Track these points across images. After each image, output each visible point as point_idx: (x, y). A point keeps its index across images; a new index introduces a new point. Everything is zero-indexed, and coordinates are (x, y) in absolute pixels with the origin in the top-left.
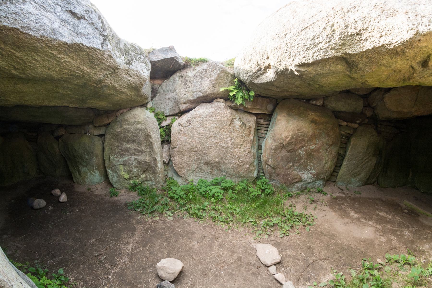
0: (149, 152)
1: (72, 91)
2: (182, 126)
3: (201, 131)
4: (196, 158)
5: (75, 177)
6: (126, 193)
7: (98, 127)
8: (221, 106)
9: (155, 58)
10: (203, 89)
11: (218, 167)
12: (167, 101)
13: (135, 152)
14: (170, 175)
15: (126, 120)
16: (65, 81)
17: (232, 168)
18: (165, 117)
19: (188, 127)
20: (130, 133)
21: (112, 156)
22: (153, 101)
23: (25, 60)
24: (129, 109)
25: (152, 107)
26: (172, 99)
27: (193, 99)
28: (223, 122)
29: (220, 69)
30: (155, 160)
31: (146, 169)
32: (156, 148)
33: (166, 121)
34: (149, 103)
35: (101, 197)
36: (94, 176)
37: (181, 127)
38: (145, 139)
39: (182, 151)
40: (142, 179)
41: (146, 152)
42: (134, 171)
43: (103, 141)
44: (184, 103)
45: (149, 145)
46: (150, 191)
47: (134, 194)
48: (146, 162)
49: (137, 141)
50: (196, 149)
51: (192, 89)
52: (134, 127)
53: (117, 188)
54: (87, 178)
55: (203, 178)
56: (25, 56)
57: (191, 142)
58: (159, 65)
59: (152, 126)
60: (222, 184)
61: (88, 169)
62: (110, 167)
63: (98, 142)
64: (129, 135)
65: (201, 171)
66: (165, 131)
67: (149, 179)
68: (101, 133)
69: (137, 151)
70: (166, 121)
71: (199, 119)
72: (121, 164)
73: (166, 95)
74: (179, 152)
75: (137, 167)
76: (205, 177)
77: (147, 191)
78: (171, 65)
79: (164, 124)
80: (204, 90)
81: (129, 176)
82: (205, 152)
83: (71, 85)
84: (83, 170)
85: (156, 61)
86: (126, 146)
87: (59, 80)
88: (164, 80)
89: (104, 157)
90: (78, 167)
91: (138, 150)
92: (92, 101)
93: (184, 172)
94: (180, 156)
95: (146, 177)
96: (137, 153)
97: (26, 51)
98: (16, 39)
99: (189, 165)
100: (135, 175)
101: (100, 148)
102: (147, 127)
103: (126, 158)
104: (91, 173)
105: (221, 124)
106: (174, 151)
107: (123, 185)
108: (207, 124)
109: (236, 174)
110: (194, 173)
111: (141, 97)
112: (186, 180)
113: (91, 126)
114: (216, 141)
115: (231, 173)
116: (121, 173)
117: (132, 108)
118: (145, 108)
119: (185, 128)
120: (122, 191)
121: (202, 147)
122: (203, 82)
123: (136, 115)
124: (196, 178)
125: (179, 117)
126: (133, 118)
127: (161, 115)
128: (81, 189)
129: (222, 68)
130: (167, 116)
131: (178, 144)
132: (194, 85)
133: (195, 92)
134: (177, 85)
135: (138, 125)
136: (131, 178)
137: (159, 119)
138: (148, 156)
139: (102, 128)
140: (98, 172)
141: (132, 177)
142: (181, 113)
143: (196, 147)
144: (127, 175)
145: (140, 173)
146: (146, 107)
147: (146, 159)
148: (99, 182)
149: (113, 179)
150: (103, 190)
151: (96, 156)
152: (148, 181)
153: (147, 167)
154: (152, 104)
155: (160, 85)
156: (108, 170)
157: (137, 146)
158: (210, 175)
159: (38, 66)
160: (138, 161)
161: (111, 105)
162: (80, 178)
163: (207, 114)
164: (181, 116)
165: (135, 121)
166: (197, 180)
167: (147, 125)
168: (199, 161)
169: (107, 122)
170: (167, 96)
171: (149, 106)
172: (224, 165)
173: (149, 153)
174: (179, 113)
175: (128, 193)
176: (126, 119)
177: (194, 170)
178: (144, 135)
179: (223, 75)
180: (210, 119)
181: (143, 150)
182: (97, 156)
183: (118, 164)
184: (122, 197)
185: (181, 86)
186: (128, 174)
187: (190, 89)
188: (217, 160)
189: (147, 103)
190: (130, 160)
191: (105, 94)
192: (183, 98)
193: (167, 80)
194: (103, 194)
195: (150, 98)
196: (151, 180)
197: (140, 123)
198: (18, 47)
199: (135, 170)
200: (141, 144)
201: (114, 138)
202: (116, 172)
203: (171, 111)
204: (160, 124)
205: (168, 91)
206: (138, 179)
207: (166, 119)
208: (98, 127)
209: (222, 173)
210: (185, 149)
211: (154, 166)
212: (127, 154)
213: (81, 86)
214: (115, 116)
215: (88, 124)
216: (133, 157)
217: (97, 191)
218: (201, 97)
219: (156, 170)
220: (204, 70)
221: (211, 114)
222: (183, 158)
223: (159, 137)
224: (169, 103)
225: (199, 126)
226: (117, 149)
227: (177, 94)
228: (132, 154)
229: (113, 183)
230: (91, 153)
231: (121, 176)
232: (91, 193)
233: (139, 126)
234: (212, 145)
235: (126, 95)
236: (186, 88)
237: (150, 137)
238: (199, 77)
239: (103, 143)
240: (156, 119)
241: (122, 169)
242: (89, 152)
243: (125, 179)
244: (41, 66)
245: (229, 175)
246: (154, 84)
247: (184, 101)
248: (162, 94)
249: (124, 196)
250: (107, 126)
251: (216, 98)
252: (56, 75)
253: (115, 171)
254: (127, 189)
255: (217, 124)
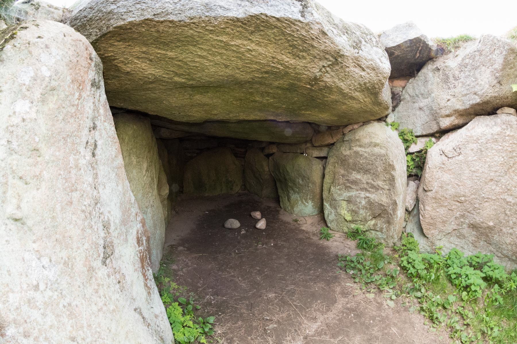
0: (388, 190)
1: (274, 98)
2: (446, 156)
3: (477, 168)
4: (458, 213)
5: (283, 201)
6: (342, 240)
7: (319, 146)
8: (511, 121)
9: (391, 42)
10: (481, 88)
11: (488, 236)
12: (418, 112)
13: (367, 187)
14: (409, 230)
15: (358, 140)
16: (260, 83)
17: (510, 244)
18: (414, 138)
19: (457, 158)
20: (363, 159)
21: (334, 186)
22: (395, 112)
23: (184, 60)
24: (361, 124)
25: (394, 122)
26: (425, 108)
27: (464, 108)
28: (514, 154)
29: (506, 47)
30: (395, 203)
31: (379, 215)
32: (399, 186)
33: (416, 144)
34: (389, 116)
35: (307, 235)
36: (306, 206)
37: (443, 157)
38: (385, 170)
39: (440, 199)
40: (369, 226)
41: (383, 189)
42: (361, 213)
43: (324, 166)
44: (448, 116)
45: (390, 180)
46: (375, 246)
47: (352, 243)
48: (381, 205)
49: (372, 171)
50: (463, 199)
51: (459, 89)
52: (369, 151)
53: (332, 228)
54: (297, 206)
55: (458, 249)
56: (182, 54)
57: (457, 185)
58: (399, 54)
59: (396, 151)
60: (486, 269)
61: (300, 197)
62: (328, 201)
63: (317, 167)
64: (361, 162)
65: (460, 235)
66: (413, 160)
67: (378, 229)
68: (323, 154)
69: (370, 185)
70: (416, 144)
71: (475, 145)
72: (345, 200)
73: (414, 102)
74: (435, 198)
75: (366, 208)
76: (462, 247)
77: (371, 245)
78: (416, 53)
79: (414, 148)
80: (483, 91)
81: (352, 218)
82: (475, 206)
83: (271, 89)
84: (294, 197)
85: (393, 47)
86: (355, 176)
87: (249, 82)
88: (408, 80)
89: (322, 186)
90: (289, 192)
91: (372, 185)
92: (308, 113)
93: (433, 231)
94: (435, 205)
95: (375, 225)
96: (370, 189)
97: (180, 46)
98: (155, 34)
99: (444, 222)
100: (360, 219)
101: (320, 174)
102: (388, 152)
103: (353, 193)
104: (302, 202)
105: (511, 158)
106: (427, 195)
107: (341, 226)
108: (487, 156)
109: (512, 256)
110: (448, 236)
111: (380, 106)
112: (433, 244)
113: (309, 145)
114: (498, 189)
115: (505, 252)
116: (342, 211)
117: (366, 122)
118: (384, 123)
119: (450, 160)
120: (337, 235)
121: (473, 196)
122: (478, 76)
123: (372, 133)
124: (447, 245)
125: (438, 138)
126: (368, 137)
127: (408, 134)
128: (285, 217)
129: (508, 45)
130: (417, 137)
131: (435, 186)
132: (462, 82)
133: (466, 95)
134: (432, 84)
135: (375, 148)
136: (353, 221)
137: (405, 141)
138: (385, 196)
139: (323, 148)
140: (312, 203)
141: (356, 221)
142: (442, 132)
143: (464, 196)
144: (349, 216)
145: (368, 218)
146: (385, 121)
147: (382, 201)
148: (311, 215)
149: (330, 216)
150: (312, 226)
151: (313, 183)
152: (377, 231)
153: (380, 212)
154: (393, 116)
155: (404, 88)
156: (325, 203)
157: (371, 178)
158: (471, 245)
159: (207, 64)
160: (369, 201)
161: (336, 118)
162: (288, 204)
163: (489, 136)
164: (440, 137)
165: (371, 143)
166: (448, 249)
167: (388, 149)
168: (462, 220)
169: (331, 141)
170: (416, 105)
171: (389, 120)
172: (499, 235)
173: (388, 192)
174: (437, 132)
175: (344, 240)
176: (357, 138)
177: (450, 232)
178: (384, 163)
179: (512, 58)
180: (494, 147)
181: (379, 186)
182: (314, 183)
183: (341, 199)
184: (335, 243)
185: (440, 87)
186: (351, 215)
187: (456, 90)
188: (491, 224)
189: (386, 116)
190: (358, 197)
191: (327, 101)
192: (445, 107)
193: (413, 78)
194: (311, 231)
195: (391, 108)
196: (381, 231)
197: (378, 145)
198: (166, 44)
199: (361, 212)
200: (378, 176)
201: (340, 163)
202: (335, 208)
203: (424, 129)
204: (406, 149)
205: (417, 96)
206: (364, 225)
207: (416, 141)
208: (319, 146)
209: (491, 248)
210: (445, 195)
211: (392, 212)
212: (355, 187)
213: (287, 89)
214: (342, 134)
215: (306, 142)
216: (363, 193)
217: (305, 225)
218: (478, 104)
219: (393, 219)
220: (477, 53)
221: (496, 137)
222: (438, 210)
223: (405, 168)
224: (421, 116)
225: (475, 158)
226: (343, 180)
227: (433, 101)
228: (362, 189)
229: (328, 221)
230: (306, 179)
231: (341, 215)
232: (297, 226)
233: (377, 150)
234: (490, 197)
235: (358, 102)
236: (449, 88)
237: (393, 168)
238: (468, 67)
239: (324, 168)
240: (401, 141)
241: (345, 207)
242: (304, 177)
243: (346, 220)
244: (211, 64)
245: (500, 255)
246: (394, 87)
247: (448, 112)
248: (408, 102)
249: (338, 243)
250: (331, 147)
251: (501, 106)
252: (242, 75)
253: (334, 207)
254: (344, 233)
255: (505, 157)
